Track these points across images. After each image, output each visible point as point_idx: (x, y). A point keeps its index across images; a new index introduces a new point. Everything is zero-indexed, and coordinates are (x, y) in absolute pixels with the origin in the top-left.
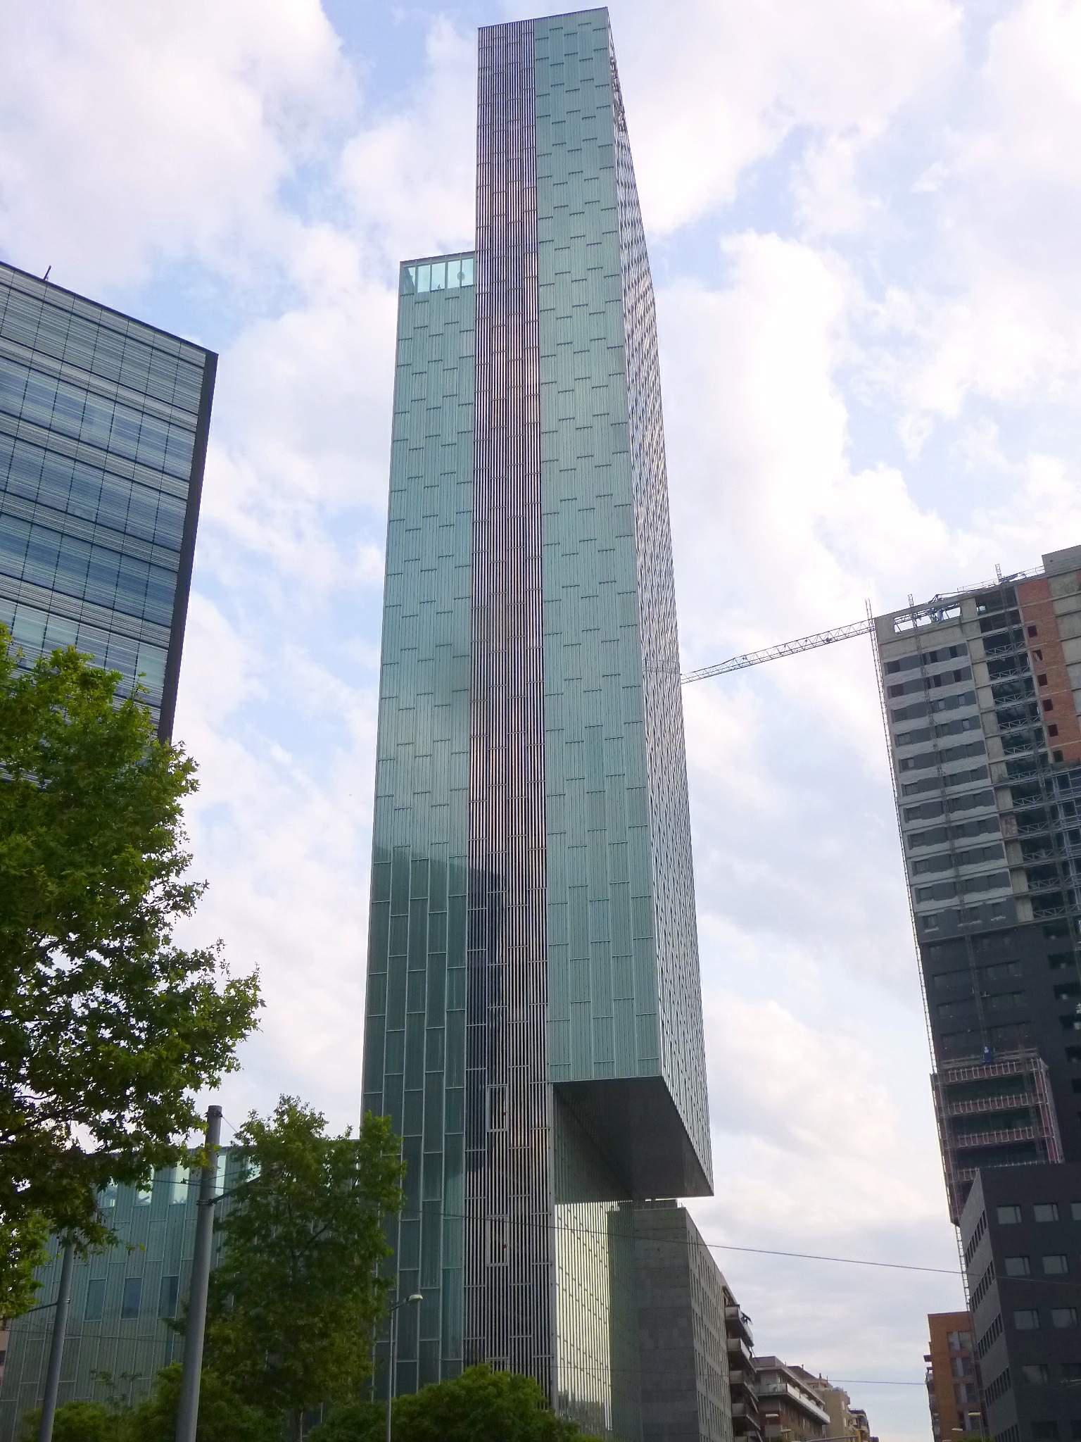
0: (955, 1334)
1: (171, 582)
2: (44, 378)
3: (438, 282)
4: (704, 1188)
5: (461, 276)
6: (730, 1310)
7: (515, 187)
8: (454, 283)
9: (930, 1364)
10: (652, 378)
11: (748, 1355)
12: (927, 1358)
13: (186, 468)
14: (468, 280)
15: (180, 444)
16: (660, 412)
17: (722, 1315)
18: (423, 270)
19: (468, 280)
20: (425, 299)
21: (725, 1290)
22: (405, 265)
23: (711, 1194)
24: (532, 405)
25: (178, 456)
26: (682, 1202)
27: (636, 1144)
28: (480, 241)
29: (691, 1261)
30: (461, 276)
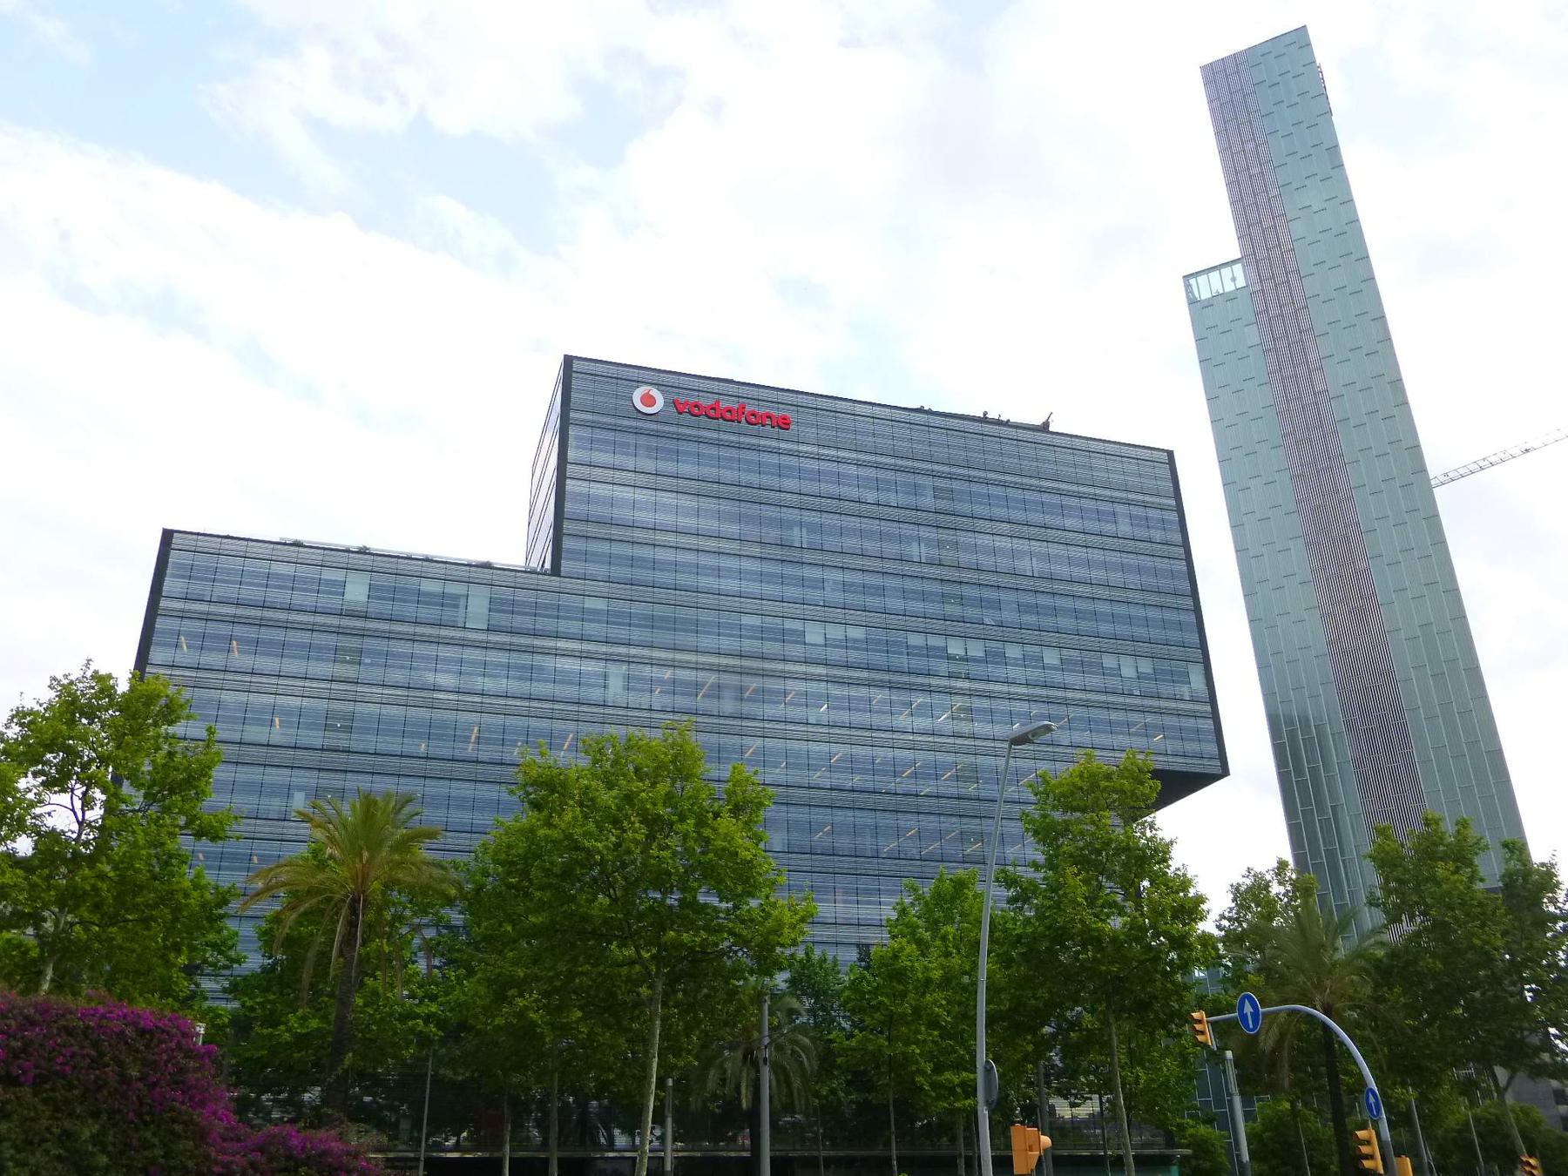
1: (1192, 618)
2: (349, 638)
3: (1217, 287)
5: (1234, 279)
7: (1262, 198)
8: (1230, 287)
14: (1241, 282)
15: (1171, 522)
18: (1202, 279)
19: (1241, 282)
20: (1209, 304)
22: (1186, 278)
24: (1316, 376)
25: (709, 633)
28: (1242, 247)
30: (1234, 279)
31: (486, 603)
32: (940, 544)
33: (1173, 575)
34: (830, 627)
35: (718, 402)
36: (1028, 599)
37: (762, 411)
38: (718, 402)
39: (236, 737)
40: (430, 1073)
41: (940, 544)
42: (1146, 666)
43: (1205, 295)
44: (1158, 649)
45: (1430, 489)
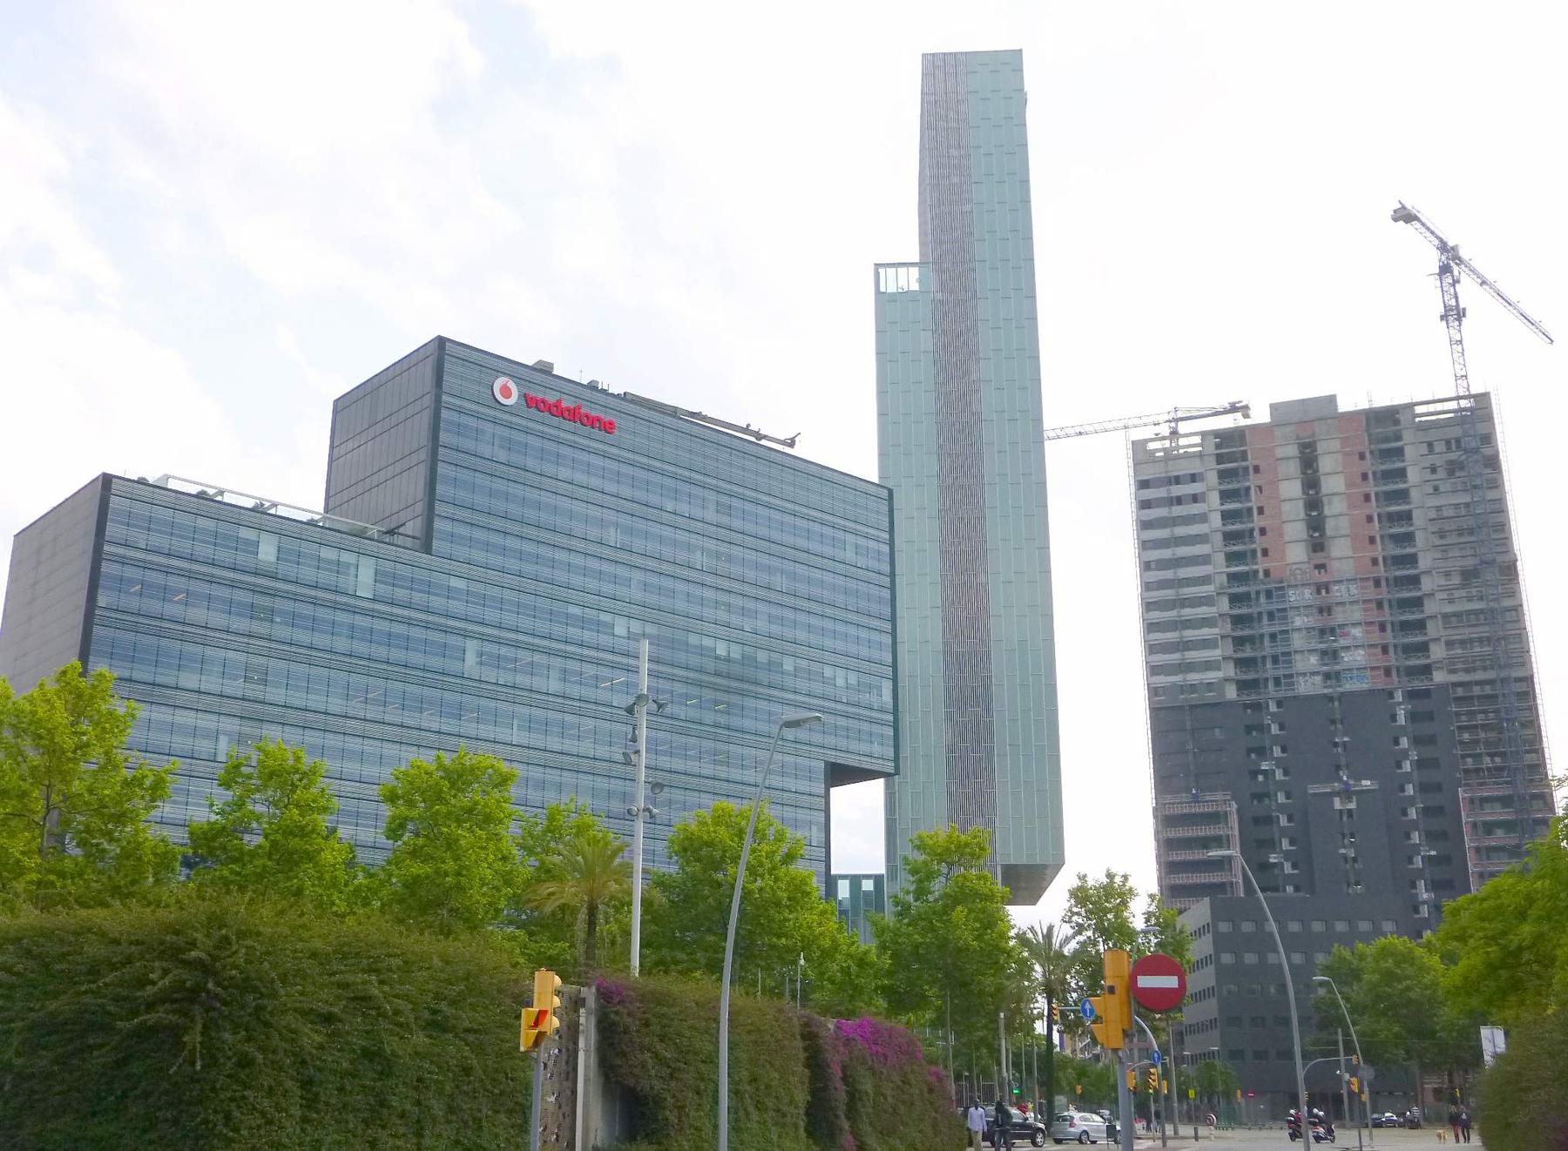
31: (371, 573)
32: (718, 556)
33: (880, 600)
34: (632, 622)
35: (559, 402)
36: (653, 579)
37: (594, 414)
38: (559, 402)
39: (150, 679)
40: (639, 865)
41: (718, 556)
42: (853, 678)
43: (892, 289)
44: (865, 666)
45: (1040, 442)
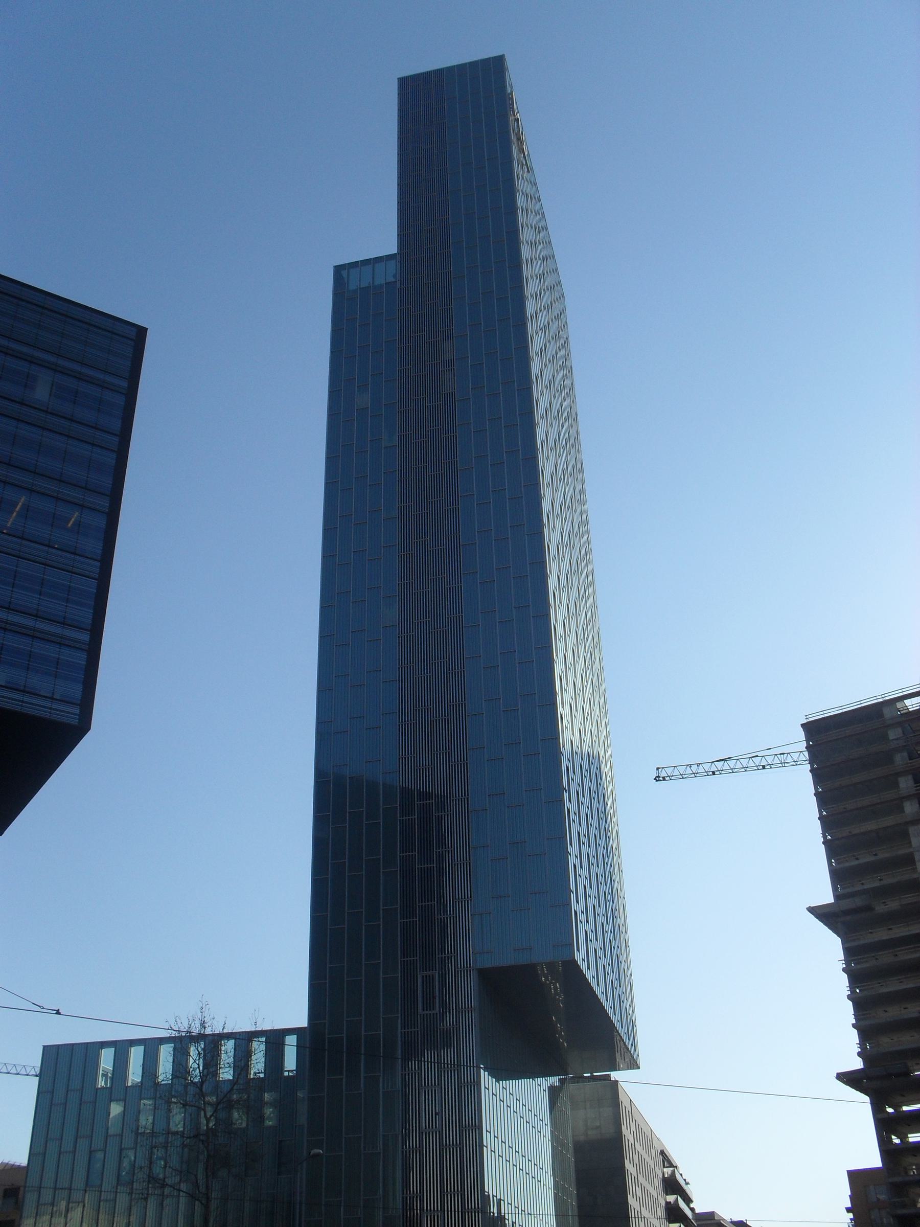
0: (872, 1188)
4: (634, 1065)
6: (668, 1171)
8: (380, 281)
9: (851, 1215)
10: (566, 408)
11: (689, 1214)
12: (848, 1210)
13: (116, 425)
16: (577, 438)
17: (661, 1176)
21: (662, 1153)
23: (639, 1068)
26: (615, 1075)
27: (566, 1026)
29: (624, 1128)
